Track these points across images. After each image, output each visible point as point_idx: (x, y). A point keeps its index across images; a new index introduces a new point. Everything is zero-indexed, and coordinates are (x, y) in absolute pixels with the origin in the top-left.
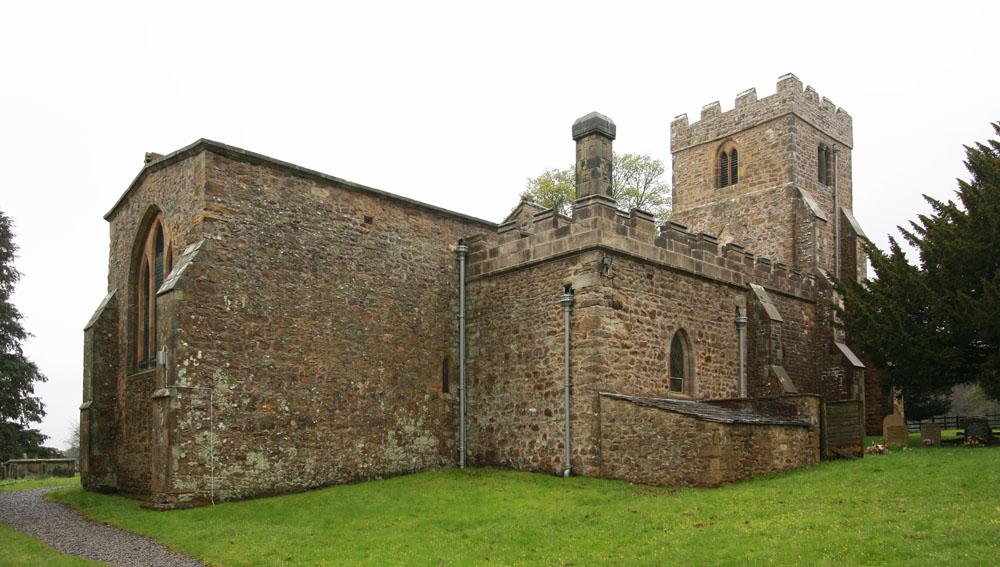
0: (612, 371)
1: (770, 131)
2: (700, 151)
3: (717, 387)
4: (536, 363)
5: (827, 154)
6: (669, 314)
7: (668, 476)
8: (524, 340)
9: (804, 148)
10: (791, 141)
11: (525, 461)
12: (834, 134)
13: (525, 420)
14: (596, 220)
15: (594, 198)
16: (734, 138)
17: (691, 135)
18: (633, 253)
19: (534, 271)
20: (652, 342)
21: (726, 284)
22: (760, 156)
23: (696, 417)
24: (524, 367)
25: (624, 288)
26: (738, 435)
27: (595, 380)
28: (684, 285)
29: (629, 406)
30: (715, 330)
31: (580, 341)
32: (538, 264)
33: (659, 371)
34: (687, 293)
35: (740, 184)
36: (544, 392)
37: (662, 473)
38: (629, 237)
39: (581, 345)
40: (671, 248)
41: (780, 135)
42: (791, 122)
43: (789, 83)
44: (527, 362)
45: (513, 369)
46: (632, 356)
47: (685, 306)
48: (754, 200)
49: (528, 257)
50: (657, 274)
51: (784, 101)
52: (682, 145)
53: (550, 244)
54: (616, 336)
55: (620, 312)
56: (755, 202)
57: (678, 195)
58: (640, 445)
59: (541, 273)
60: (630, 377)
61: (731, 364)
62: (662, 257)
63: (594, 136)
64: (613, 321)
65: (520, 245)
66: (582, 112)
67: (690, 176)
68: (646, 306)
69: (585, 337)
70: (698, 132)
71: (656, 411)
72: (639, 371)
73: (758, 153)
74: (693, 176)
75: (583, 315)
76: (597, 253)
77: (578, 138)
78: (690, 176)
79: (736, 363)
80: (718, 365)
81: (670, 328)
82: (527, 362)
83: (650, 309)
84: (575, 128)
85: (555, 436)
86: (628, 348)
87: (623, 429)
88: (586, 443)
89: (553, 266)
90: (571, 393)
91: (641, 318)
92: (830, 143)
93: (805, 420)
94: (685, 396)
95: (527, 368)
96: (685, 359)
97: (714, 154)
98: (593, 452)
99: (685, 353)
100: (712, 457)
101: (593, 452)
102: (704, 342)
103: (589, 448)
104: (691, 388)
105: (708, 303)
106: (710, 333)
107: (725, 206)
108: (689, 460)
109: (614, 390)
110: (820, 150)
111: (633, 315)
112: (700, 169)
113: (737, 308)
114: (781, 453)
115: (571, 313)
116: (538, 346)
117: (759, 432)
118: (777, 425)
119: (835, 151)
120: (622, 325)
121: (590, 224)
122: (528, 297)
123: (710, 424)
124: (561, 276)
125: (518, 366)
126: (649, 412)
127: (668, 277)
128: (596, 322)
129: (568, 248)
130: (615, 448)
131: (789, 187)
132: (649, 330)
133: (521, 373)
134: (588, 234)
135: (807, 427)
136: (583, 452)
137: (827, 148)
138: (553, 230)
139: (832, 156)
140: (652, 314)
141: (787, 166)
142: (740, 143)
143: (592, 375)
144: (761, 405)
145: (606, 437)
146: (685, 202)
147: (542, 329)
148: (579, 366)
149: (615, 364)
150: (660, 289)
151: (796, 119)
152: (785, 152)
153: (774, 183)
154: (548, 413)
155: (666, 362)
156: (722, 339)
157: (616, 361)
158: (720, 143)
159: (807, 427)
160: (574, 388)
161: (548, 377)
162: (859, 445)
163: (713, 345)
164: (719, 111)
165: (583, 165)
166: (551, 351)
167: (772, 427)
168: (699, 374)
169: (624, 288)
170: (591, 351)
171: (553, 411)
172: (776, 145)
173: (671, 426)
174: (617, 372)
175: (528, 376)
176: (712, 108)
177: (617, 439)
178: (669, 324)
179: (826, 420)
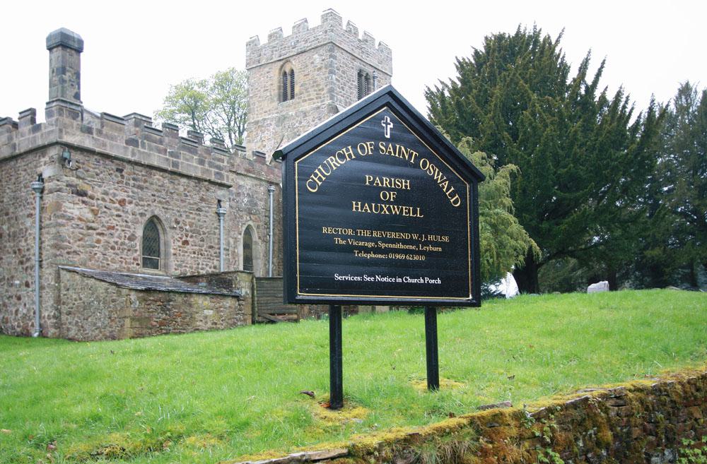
0: (75, 248)
1: (316, 56)
2: (267, 69)
3: (195, 266)
4: (19, 241)
5: (367, 79)
6: (141, 203)
7: (101, 335)
8: (13, 221)
9: (344, 72)
10: (331, 66)
11: (13, 328)
12: (374, 62)
13: (13, 291)
14: (57, 120)
15: (56, 101)
16: (291, 59)
17: (260, 55)
18: (97, 150)
19: (19, 161)
20: (121, 226)
21: (206, 181)
22: (310, 77)
23: (116, 284)
24: (12, 245)
25: (89, 179)
26: (152, 300)
27: (56, 256)
28: (159, 180)
29: (77, 277)
30: (194, 218)
31: (48, 222)
32: (20, 155)
33: (129, 250)
34: (162, 186)
35: (296, 100)
36: (25, 266)
37: (97, 332)
38: (95, 136)
39: (48, 226)
40: (143, 146)
41: (323, 60)
42: (332, 50)
43: (331, 16)
44: (14, 241)
45: (5, 247)
46: (98, 237)
47: (158, 197)
48: (305, 114)
49: (15, 149)
50: (128, 168)
51: (326, 32)
52: (254, 63)
53: (29, 139)
54: (80, 219)
55: (85, 199)
56: (306, 116)
57: (252, 107)
58: (84, 310)
59: (23, 164)
60: (96, 254)
61: (211, 247)
62: (133, 154)
63: (60, 48)
64: (78, 206)
65: (10, 139)
66: (53, 27)
67: (260, 91)
68: (115, 195)
69: (50, 219)
70: (266, 52)
71: (93, 280)
72: (106, 249)
73: (308, 75)
74: (262, 90)
75: (49, 199)
76: (58, 147)
77: (50, 49)
78: (260, 91)
79: (217, 246)
80: (197, 248)
81: (141, 215)
82: (14, 241)
83: (119, 198)
84: (48, 39)
85: (31, 304)
86: (95, 229)
87: (75, 296)
88: (50, 310)
89: (30, 157)
90: (41, 266)
91: (108, 204)
92: (370, 70)
93: (237, 291)
94: (161, 273)
95: (14, 246)
96: (162, 242)
97: (277, 71)
98: (54, 317)
99: (162, 236)
100: (125, 317)
101: (54, 317)
102: (181, 228)
103: (52, 314)
104: (166, 266)
105: (187, 196)
106: (187, 221)
107: (285, 118)
108: (112, 321)
109: (78, 264)
110: (360, 75)
111: (100, 202)
112: (267, 84)
113: (219, 201)
114: (206, 317)
115: (41, 198)
116: (21, 227)
117: (179, 299)
118: (198, 294)
119: (374, 77)
120: (87, 210)
121: (53, 123)
122: (15, 184)
123: (124, 290)
124: (36, 167)
125: (8, 244)
126: (89, 282)
127: (141, 172)
128: (58, 206)
129: (40, 142)
130: (69, 313)
131: (330, 105)
132: (119, 216)
133: (10, 250)
134: (52, 131)
135: (237, 297)
136: (49, 317)
137: (367, 74)
138: (31, 126)
139: (372, 81)
140: (122, 202)
141: (328, 87)
142: (295, 65)
143: (54, 251)
144: (212, 280)
145: (64, 303)
146: (256, 112)
147: (24, 212)
148: (47, 243)
149: (78, 243)
150: (132, 182)
151: (336, 48)
152: (327, 75)
153: (319, 100)
154: (27, 285)
155: (138, 244)
156: (201, 227)
157: (79, 240)
158: (281, 63)
159: (237, 297)
160: (44, 262)
161: (27, 253)
162: (296, 314)
163: (191, 231)
164: (280, 36)
165: (53, 72)
166: (29, 231)
167: (194, 295)
168: (175, 254)
169: (89, 179)
170: (53, 230)
171: (30, 283)
172: (320, 68)
173: (102, 293)
174: (81, 250)
175: (15, 253)
176: (276, 33)
177: (71, 305)
178: (141, 211)
179: (255, 292)
